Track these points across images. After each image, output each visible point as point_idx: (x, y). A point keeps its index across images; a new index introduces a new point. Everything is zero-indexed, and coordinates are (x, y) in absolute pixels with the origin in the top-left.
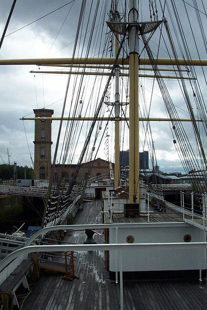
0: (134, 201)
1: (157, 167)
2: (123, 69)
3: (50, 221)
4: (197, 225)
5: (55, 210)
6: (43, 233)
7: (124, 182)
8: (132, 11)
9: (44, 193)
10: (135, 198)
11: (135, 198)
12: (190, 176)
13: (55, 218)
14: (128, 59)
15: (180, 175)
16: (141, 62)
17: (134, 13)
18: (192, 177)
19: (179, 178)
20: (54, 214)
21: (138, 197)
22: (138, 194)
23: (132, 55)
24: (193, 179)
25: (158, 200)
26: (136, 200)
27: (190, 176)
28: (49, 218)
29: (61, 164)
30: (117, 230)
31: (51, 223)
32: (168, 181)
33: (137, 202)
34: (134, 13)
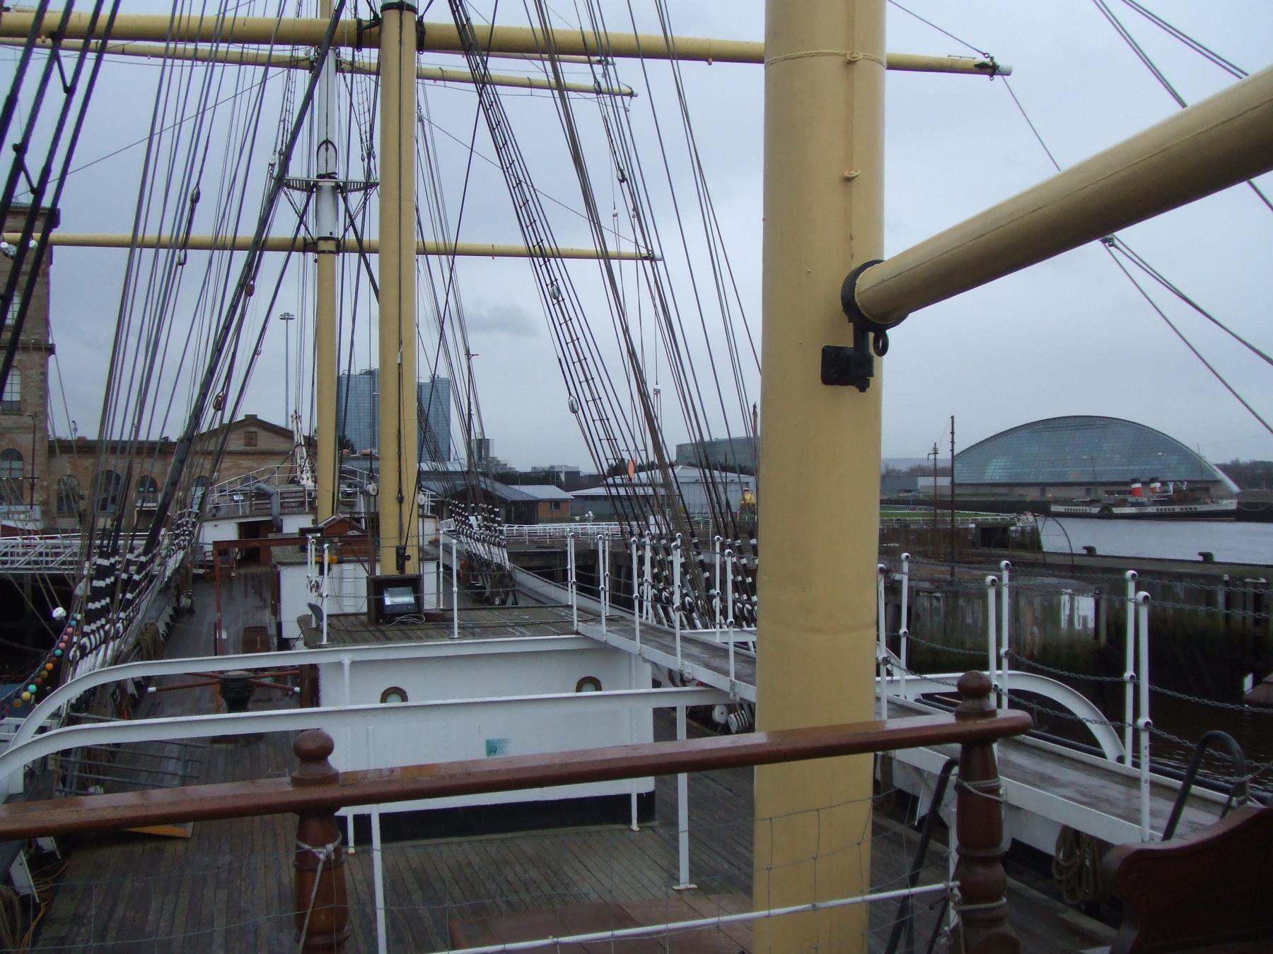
0: (401, 566)
1: (483, 444)
2: (352, 72)
3: (91, 652)
4: (616, 640)
5: (104, 612)
6: (62, 698)
7: (355, 493)
8: (324, 146)
9: (57, 554)
10: (402, 557)
11: (402, 557)
12: (616, 486)
13: (105, 641)
14: (375, 30)
15: (573, 480)
16: (425, 42)
17: (327, 149)
18: (614, 491)
19: (569, 495)
20: (103, 626)
21: (412, 551)
22: (412, 542)
23: (393, 16)
24: (628, 498)
25: (488, 564)
26: (407, 563)
27: (616, 486)
28: (85, 640)
29: (125, 438)
30: (347, 668)
31: (91, 658)
32: (526, 512)
33: (411, 568)
34: (327, 149)
